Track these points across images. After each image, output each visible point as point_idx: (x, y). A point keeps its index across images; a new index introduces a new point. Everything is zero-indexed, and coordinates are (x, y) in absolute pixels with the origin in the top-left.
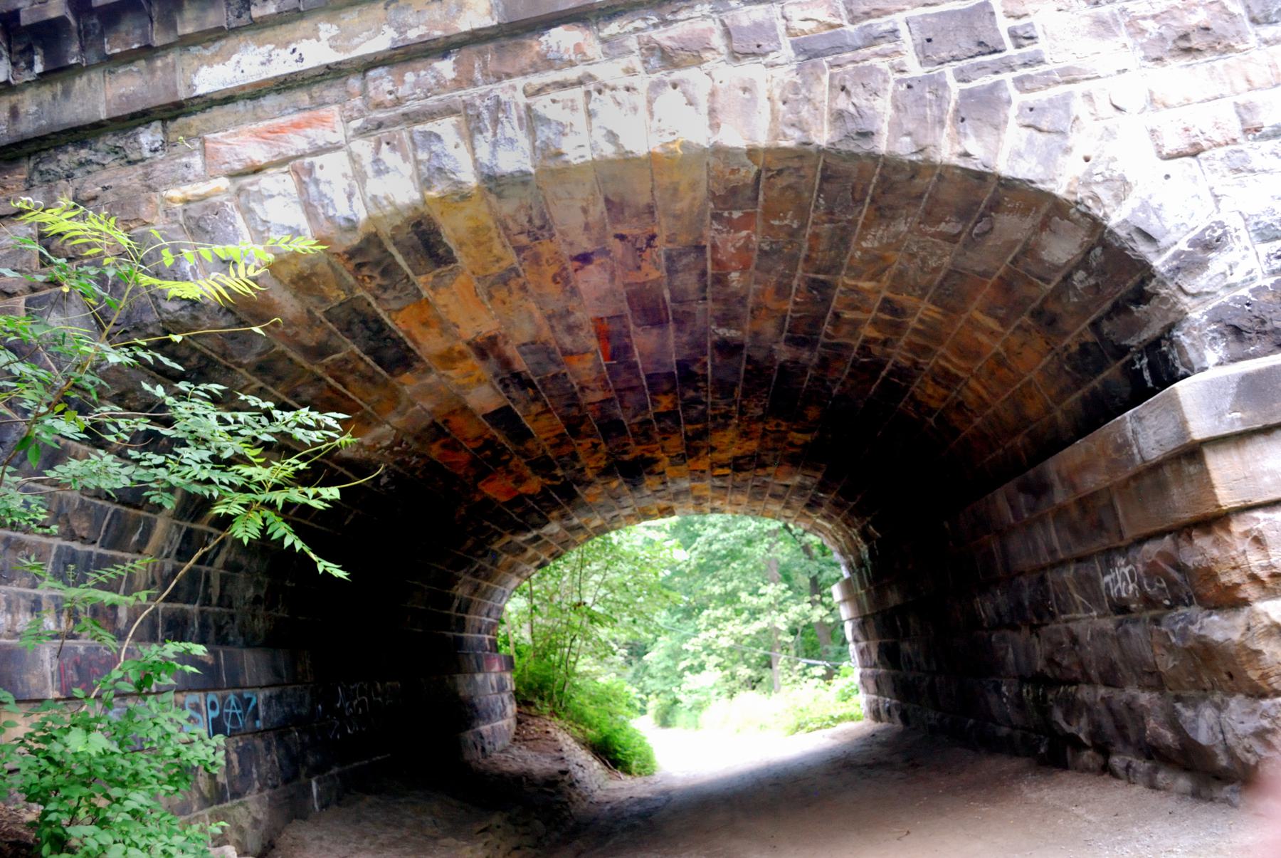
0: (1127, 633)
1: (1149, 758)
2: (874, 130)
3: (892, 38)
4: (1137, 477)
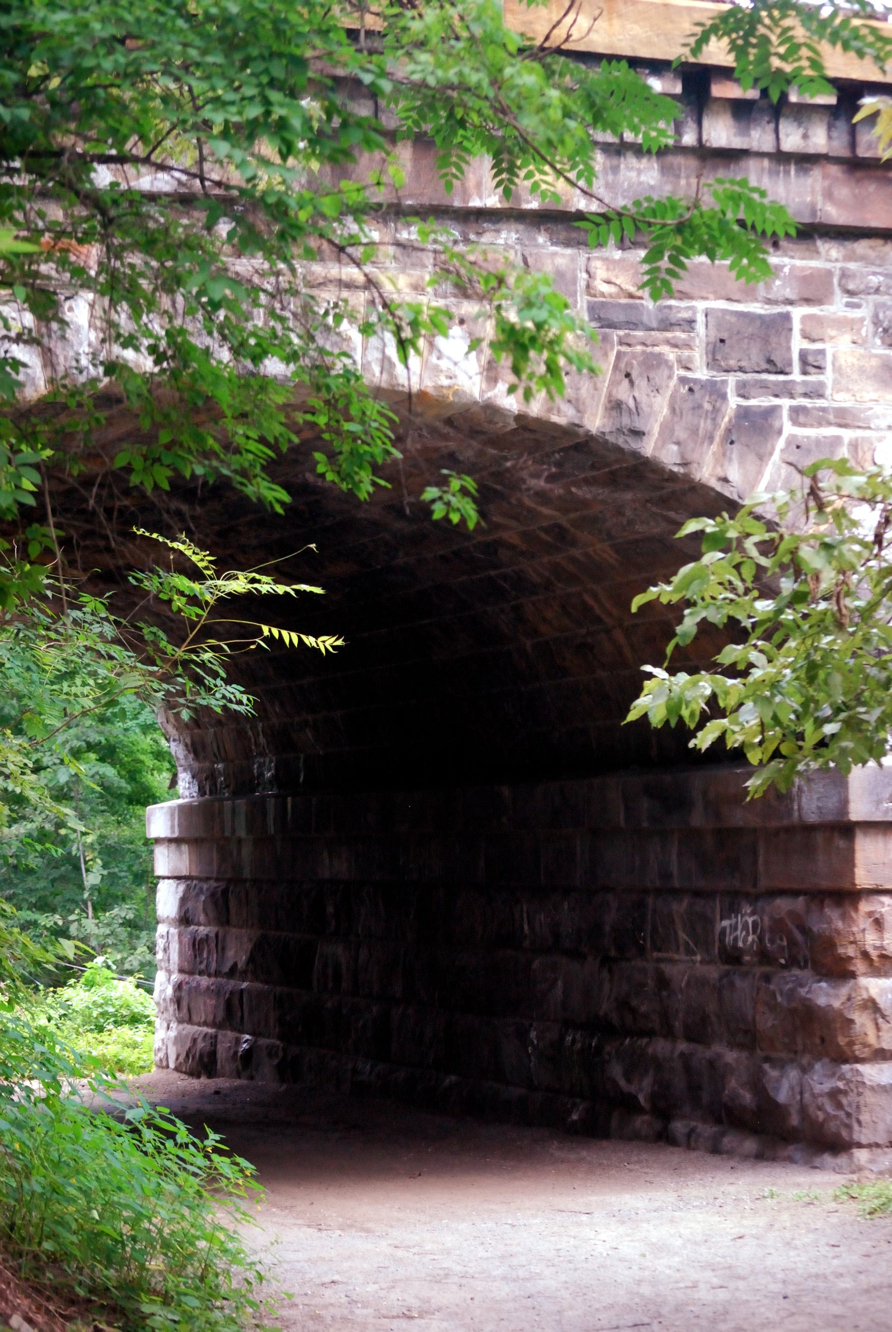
0: (732, 985)
1: (718, 1121)
2: (646, 431)
3: (687, 328)
4: (790, 830)
